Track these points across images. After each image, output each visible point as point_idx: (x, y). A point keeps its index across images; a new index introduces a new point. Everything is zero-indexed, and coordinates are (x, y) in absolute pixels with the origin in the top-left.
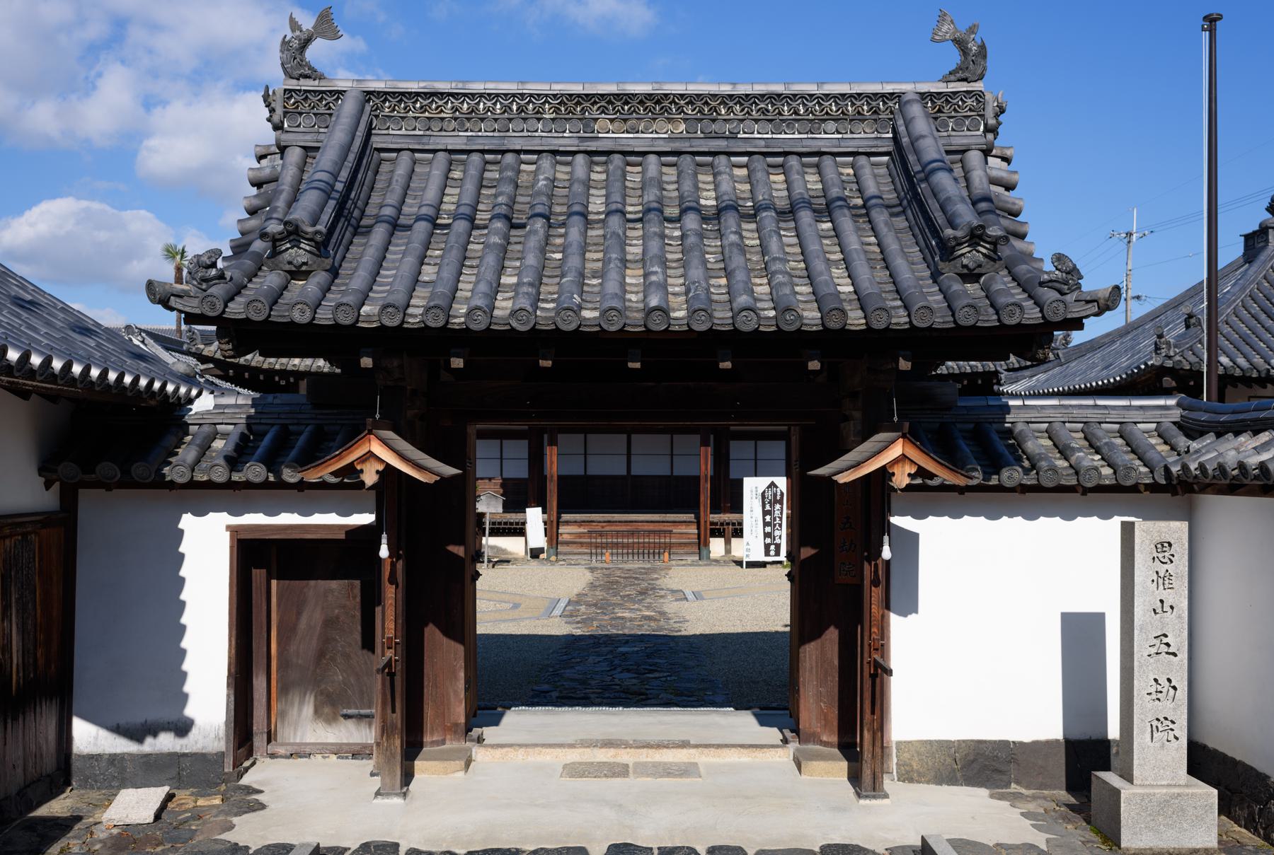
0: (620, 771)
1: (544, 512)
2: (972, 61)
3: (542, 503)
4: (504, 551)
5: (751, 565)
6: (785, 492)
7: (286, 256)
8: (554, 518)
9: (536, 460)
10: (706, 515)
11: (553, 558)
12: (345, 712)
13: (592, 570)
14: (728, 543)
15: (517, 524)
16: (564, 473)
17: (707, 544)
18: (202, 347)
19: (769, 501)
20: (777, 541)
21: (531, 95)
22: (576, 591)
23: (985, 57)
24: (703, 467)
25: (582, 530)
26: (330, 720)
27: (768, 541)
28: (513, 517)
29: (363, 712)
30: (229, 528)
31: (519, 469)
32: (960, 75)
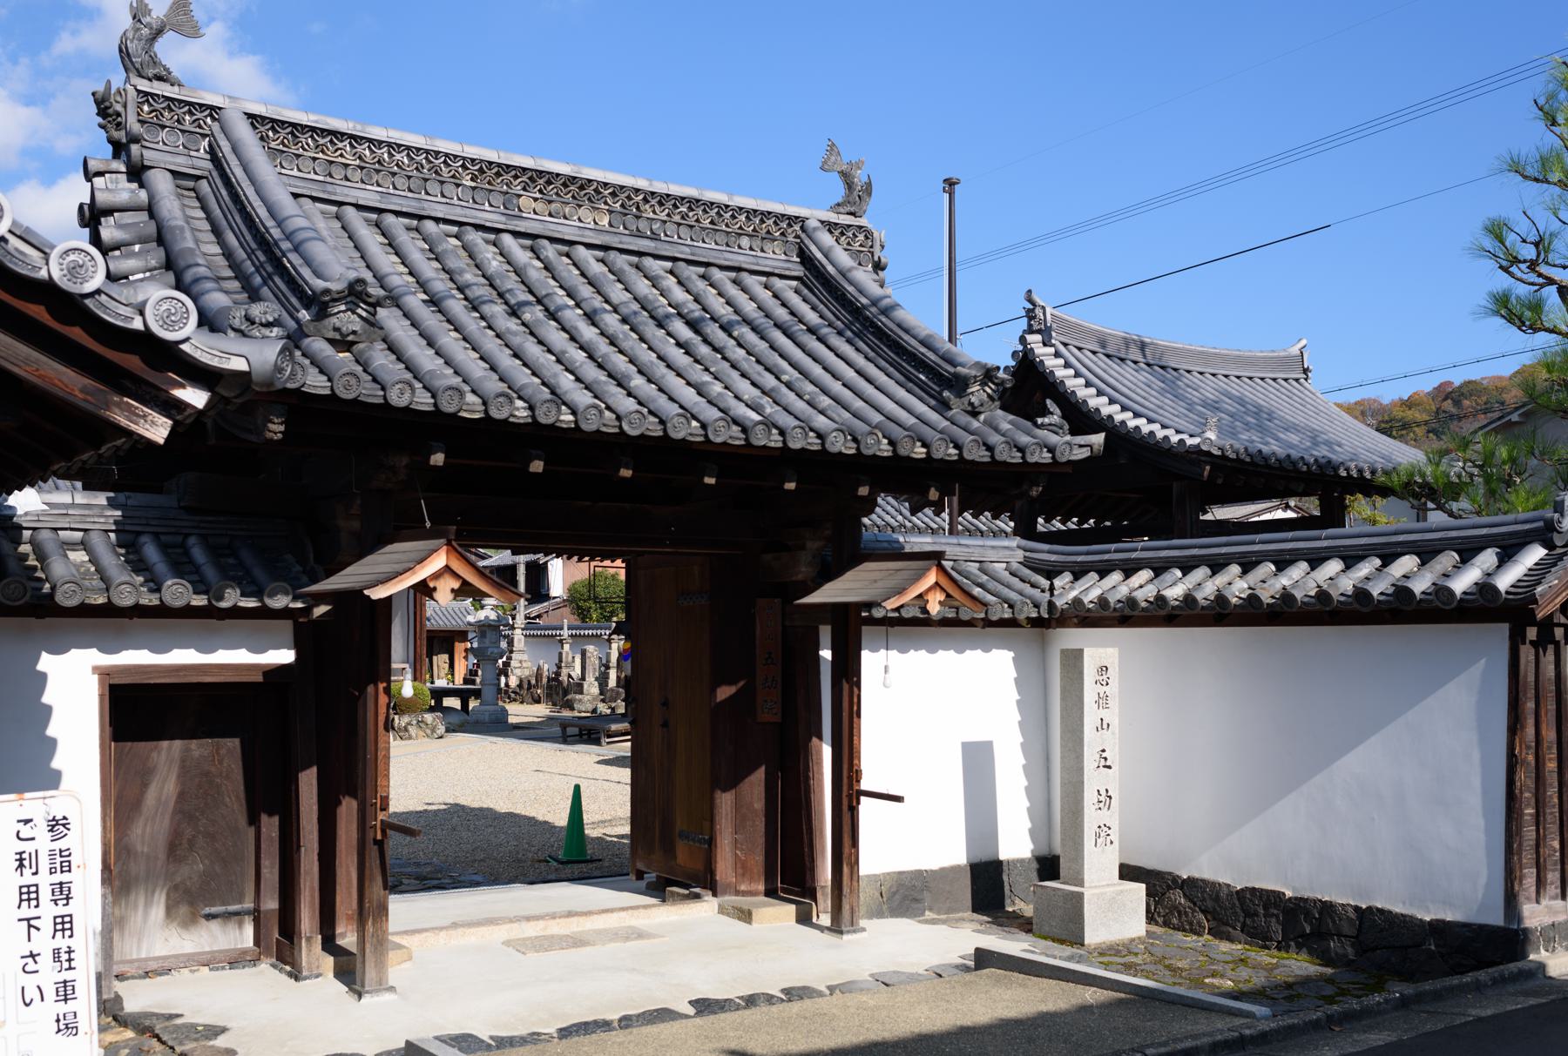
0: (577, 942)
2: (856, 194)
7: (334, 320)
12: (207, 910)
21: (447, 155)
23: (870, 194)
26: (190, 921)
29: (232, 908)
30: (96, 669)
32: (849, 209)
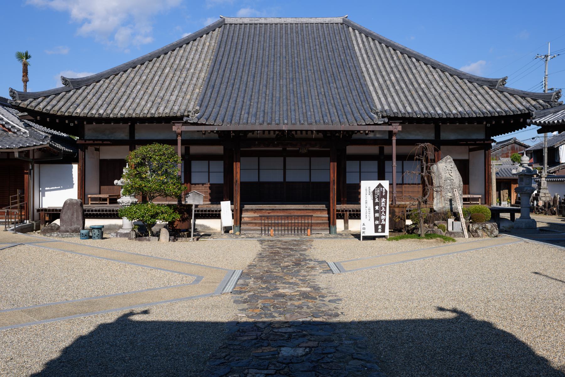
1: (231, 204)
3: (231, 199)
4: (208, 228)
5: (366, 238)
6: (388, 190)
8: (238, 207)
9: (228, 173)
10: (334, 205)
11: (238, 233)
13: (262, 242)
14: (346, 223)
15: (216, 211)
16: (243, 180)
17: (334, 224)
18: (19, 102)
19: (378, 195)
20: (383, 222)
22: (248, 262)
24: (332, 175)
25: (256, 215)
27: (377, 222)
28: (214, 207)
31: (218, 179)
